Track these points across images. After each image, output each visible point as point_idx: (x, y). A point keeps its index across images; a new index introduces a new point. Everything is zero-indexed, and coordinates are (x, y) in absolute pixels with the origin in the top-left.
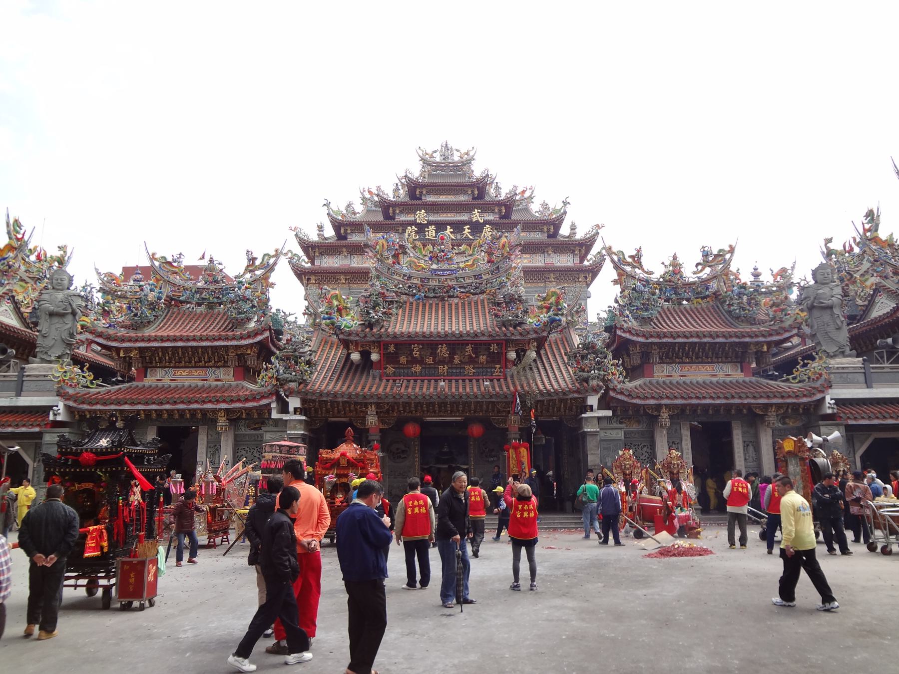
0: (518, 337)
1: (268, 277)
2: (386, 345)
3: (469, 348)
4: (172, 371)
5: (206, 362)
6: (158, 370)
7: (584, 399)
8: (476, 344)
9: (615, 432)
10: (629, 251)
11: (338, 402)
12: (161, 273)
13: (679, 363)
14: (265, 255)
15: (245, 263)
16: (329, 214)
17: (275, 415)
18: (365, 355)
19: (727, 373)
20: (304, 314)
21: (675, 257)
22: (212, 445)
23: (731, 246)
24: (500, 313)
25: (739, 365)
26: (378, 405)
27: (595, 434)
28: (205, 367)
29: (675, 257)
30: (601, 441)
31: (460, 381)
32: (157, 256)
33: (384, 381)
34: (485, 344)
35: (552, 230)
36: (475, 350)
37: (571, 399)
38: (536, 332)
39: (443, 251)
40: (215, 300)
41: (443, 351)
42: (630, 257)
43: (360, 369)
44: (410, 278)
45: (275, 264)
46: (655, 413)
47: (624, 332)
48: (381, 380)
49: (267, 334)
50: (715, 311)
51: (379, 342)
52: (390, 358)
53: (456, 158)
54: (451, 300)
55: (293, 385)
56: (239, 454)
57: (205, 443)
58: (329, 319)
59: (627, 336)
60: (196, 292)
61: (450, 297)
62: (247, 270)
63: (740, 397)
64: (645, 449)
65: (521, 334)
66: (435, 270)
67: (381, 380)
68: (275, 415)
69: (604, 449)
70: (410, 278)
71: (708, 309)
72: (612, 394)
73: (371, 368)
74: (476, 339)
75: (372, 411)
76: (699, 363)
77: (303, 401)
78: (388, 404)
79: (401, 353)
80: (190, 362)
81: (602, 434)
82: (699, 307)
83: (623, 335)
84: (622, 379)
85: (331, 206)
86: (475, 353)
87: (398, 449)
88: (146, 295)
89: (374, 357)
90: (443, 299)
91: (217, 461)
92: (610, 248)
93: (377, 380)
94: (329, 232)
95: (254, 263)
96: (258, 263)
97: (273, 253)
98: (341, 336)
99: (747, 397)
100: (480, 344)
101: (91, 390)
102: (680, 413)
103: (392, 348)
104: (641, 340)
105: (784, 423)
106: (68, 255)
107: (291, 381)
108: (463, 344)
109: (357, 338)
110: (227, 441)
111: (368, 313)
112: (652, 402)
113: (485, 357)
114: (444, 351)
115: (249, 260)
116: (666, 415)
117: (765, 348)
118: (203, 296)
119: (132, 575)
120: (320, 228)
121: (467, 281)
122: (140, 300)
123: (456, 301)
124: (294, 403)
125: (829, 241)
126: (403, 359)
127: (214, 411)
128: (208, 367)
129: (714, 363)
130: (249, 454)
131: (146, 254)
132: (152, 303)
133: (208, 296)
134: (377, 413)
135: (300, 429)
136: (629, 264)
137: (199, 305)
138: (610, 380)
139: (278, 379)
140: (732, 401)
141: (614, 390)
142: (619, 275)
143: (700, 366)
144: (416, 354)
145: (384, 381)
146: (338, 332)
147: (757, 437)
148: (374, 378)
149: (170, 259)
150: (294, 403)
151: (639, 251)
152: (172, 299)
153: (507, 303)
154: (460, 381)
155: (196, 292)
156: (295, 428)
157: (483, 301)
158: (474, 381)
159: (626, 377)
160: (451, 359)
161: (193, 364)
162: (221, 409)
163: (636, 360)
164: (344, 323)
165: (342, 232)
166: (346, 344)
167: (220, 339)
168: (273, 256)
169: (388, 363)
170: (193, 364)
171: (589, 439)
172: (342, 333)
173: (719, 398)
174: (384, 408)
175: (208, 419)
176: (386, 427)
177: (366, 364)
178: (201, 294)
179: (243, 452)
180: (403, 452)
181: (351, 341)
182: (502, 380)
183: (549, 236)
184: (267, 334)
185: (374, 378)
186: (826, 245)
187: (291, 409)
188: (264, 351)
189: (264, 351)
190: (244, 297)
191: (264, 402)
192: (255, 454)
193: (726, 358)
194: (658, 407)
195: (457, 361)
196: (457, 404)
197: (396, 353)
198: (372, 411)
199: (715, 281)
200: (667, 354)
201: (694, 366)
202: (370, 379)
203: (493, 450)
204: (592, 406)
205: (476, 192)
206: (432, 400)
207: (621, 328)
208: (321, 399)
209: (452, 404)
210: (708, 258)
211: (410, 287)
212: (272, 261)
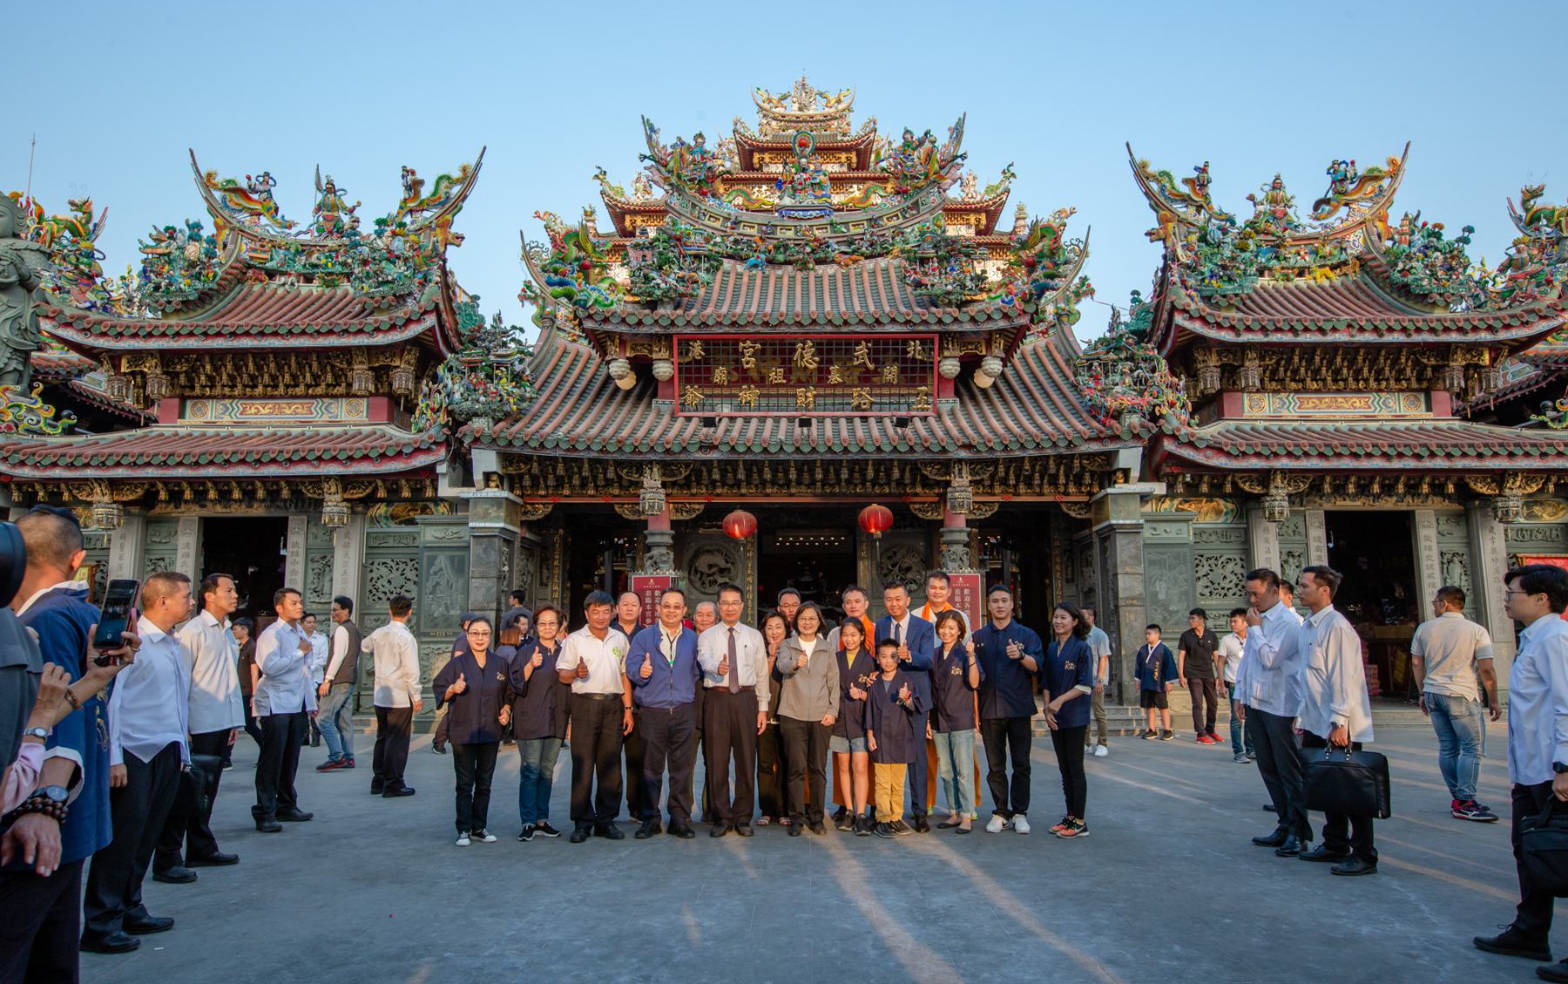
0: (968, 327)
1: (449, 224)
2: (685, 342)
3: (861, 351)
4: (238, 405)
5: (308, 386)
6: (209, 403)
7: (1111, 456)
8: (876, 342)
9: (1175, 526)
10: (1181, 172)
11: (579, 461)
12: (226, 213)
13: (1297, 391)
14: (441, 178)
15: (401, 193)
16: (602, 193)
17: (445, 490)
18: (642, 367)
19: (1391, 413)
20: (523, 298)
21: (1277, 185)
22: (318, 557)
23: (1392, 162)
24: (926, 280)
25: (1422, 397)
26: (666, 467)
27: (1135, 530)
28: (306, 396)
29: (1277, 185)
30: (1146, 545)
31: (843, 422)
32: (219, 180)
33: (681, 420)
34: (896, 342)
35: (984, 221)
36: (874, 354)
37: (1082, 456)
38: (1006, 316)
39: (804, 170)
40: (339, 268)
41: (807, 358)
42: (1186, 181)
43: (631, 400)
44: (736, 223)
45: (463, 197)
46: (1258, 490)
47: (1191, 318)
48: (673, 417)
49: (431, 321)
50: (1363, 291)
51: (669, 337)
52: (695, 373)
53: (817, 109)
54: (820, 269)
55: (479, 424)
56: (375, 575)
57: (302, 551)
58: (561, 284)
59: (1197, 327)
60: (298, 252)
61: (819, 262)
62: (406, 209)
63: (1449, 456)
64: (1230, 566)
65: (973, 320)
66: (792, 208)
67: (673, 417)
68: (445, 490)
69: (1152, 563)
70: (736, 223)
71: (1347, 288)
72: (1168, 445)
73: (655, 395)
74: (878, 329)
75: (652, 482)
76: (1338, 391)
77: (506, 458)
78: (687, 464)
79: (716, 357)
80: (276, 387)
81: (1147, 532)
82: (1326, 283)
83: (1188, 325)
84: (1185, 417)
85: (609, 178)
86: (876, 361)
87: (710, 566)
88: (181, 249)
89: (663, 369)
90: (804, 266)
91: (326, 590)
92: (1144, 166)
93: (666, 419)
94: (605, 224)
95: (417, 194)
96: (426, 192)
97: (456, 174)
98: (589, 324)
99: (1464, 455)
100: (886, 342)
101: (49, 440)
102: (1312, 485)
103: (697, 350)
104: (1227, 336)
105: (1530, 516)
106: (96, 220)
107: (476, 415)
108: (848, 344)
109: (623, 329)
110: (346, 546)
111: (647, 279)
112: (1255, 463)
113: (895, 369)
114: (807, 356)
115: (409, 188)
116: (1283, 492)
117: (1486, 358)
118: (313, 259)
119: (1030, 661)
120: (589, 214)
121: (853, 230)
122: (167, 258)
123: (831, 269)
124: (485, 461)
125: (1532, 194)
126: (720, 374)
127: (317, 481)
128: (314, 397)
129: (1371, 391)
130: (395, 575)
131: (193, 175)
132: (192, 265)
133: (323, 261)
134: (664, 485)
135: (497, 519)
136: (1185, 199)
137: (309, 279)
138: (1162, 416)
139: (450, 413)
140: (1428, 464)
141: (1174, 437)
142: (1163, 221)
143: (1340, 398)
144: (749, 362)
145: (681, 420)
146: (581, 313)
147: (1471, 543)
148: (659, 414)
149: (244, 184)
150: (485, 461)
151: (1203, 170)
152: (250, 267)
153: (941, 259)
154: (843, 422)
155: (298, 252)
156: (485, 517)
157: (886, 271)
158: (872, 421)
159: (1192, 415)
160: (823, 372)
161: (281, 389)
162: (328, 478)
163: (1211, 380)
164: (595, 295)
165: (627, 223)
166: (600, 341)
167: (330, 332)
168: (458, 181)
169: (688, 381)
170: (281, 389)
171: (1120, 541)
172: (590, 317)
173: (1400, 455)
174: (683, 472)
175: (303, 496)
176: (685, 517)
177: (647, 387)
178: (310, 254)
179: (383, 571)
180: (722, 571)
181: (610, 335)
182: (932, 420)
183: (978, 233)
184: (431, 321)
185: (659, 414)
186: (1524, 203)
187: (478, 477)
188: (426, 355)
189: (426, 355)
190: (390, 252)
191: (421, 461)
192: (409, 574)
193: (1398, 380)
194: (1265, 477)
195: (835, 378)
196: (837, 464)
197: (706, 361)
198: (652, 482)
199: (1359, 232)
200: (1274, 372)
201: (1327, 397)
202: (652, 415)
203: (909, 569)
204: (1126, 473)
205: (854, 160)
206: (782, 457)
207: (1185, 311)
208: (544, 453)
209: (826, 464)
210: (1344, 183)
211: (736, 242)
212: (456, 190)
